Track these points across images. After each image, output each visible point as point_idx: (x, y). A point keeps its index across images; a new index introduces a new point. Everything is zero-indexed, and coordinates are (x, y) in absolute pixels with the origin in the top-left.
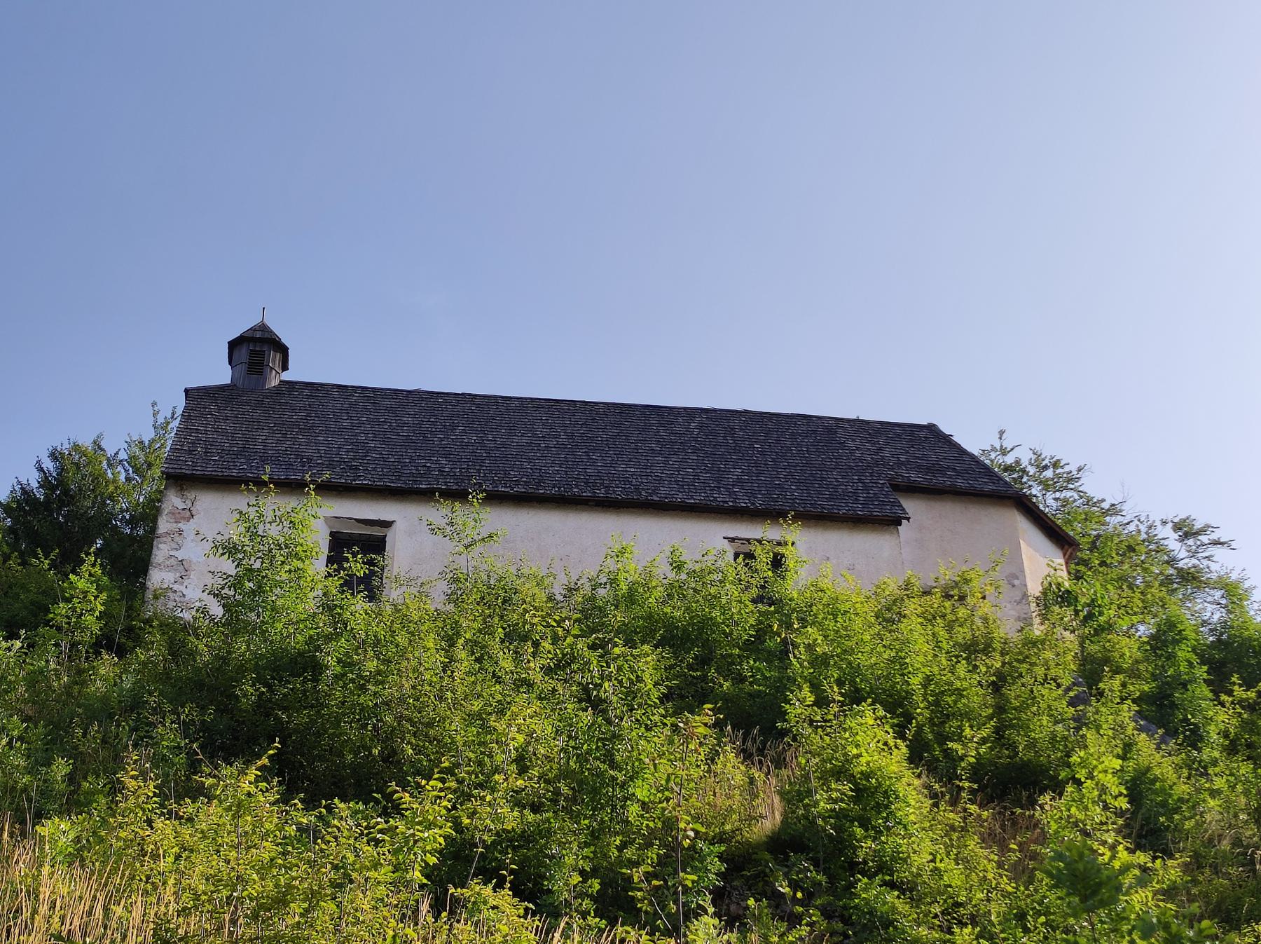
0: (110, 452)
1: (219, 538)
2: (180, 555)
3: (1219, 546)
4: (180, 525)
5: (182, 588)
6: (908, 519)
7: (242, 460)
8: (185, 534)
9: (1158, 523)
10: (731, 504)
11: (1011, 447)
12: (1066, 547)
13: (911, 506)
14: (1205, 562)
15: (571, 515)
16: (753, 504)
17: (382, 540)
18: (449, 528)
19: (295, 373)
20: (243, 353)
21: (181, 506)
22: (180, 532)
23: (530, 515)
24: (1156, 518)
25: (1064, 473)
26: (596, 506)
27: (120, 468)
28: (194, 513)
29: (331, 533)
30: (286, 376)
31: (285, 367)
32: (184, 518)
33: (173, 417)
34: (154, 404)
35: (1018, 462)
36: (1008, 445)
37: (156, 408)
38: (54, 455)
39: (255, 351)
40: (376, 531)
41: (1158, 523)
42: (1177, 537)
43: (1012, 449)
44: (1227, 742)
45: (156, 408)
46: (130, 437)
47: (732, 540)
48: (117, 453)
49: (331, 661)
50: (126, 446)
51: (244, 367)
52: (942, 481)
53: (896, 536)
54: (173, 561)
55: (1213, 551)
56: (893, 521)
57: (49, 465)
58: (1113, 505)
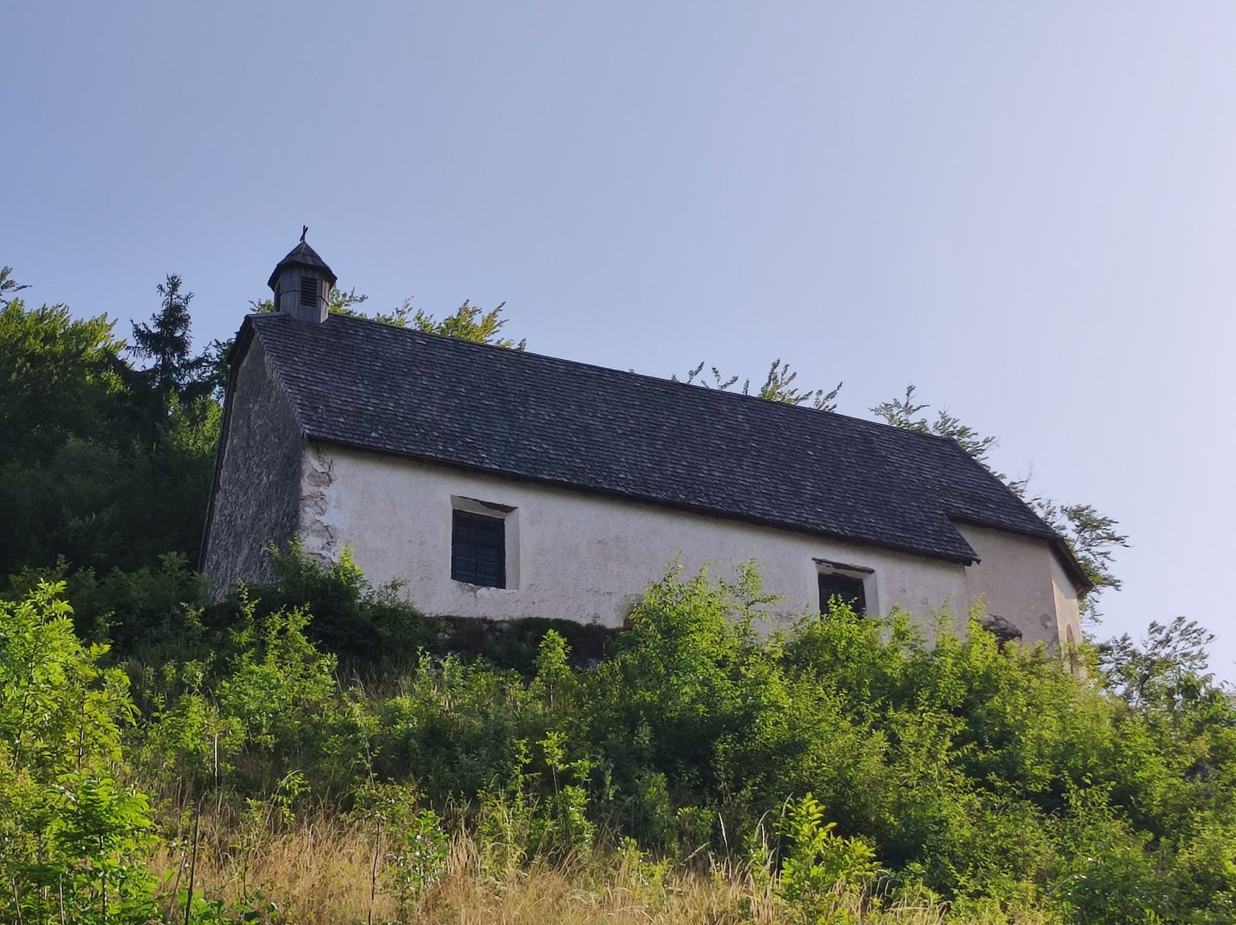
2: (325, 520)
3: (1113, 541)
4: (321, 489)
6: (978, 561)
9: (1058, 510)
11: (918, 406)
12: (1079, 586)
13: (975, 541)
14: (1101, 559)
15: (675, 519)
16: (842, 530)
17: (500, 525)
21: (320, 470)
23: (638, 516)
24: (1057, 505)
25: (970, 442)
26: (697, 513)
28: (332, 478)
29: (454, 510)
32: (323, 482)
35: (923, 423)
36: (914, 403)
39: (307, 278)
40: (496, 514)
41: (1058, 510)
42: (1075, 528)
43: (918, 408)
47: (819, 562)
51: (298, 295)
52: (986, 514)
53: (962, 571)
55: (1107, 546)
56: (962, 559)
58: (1014, 483)
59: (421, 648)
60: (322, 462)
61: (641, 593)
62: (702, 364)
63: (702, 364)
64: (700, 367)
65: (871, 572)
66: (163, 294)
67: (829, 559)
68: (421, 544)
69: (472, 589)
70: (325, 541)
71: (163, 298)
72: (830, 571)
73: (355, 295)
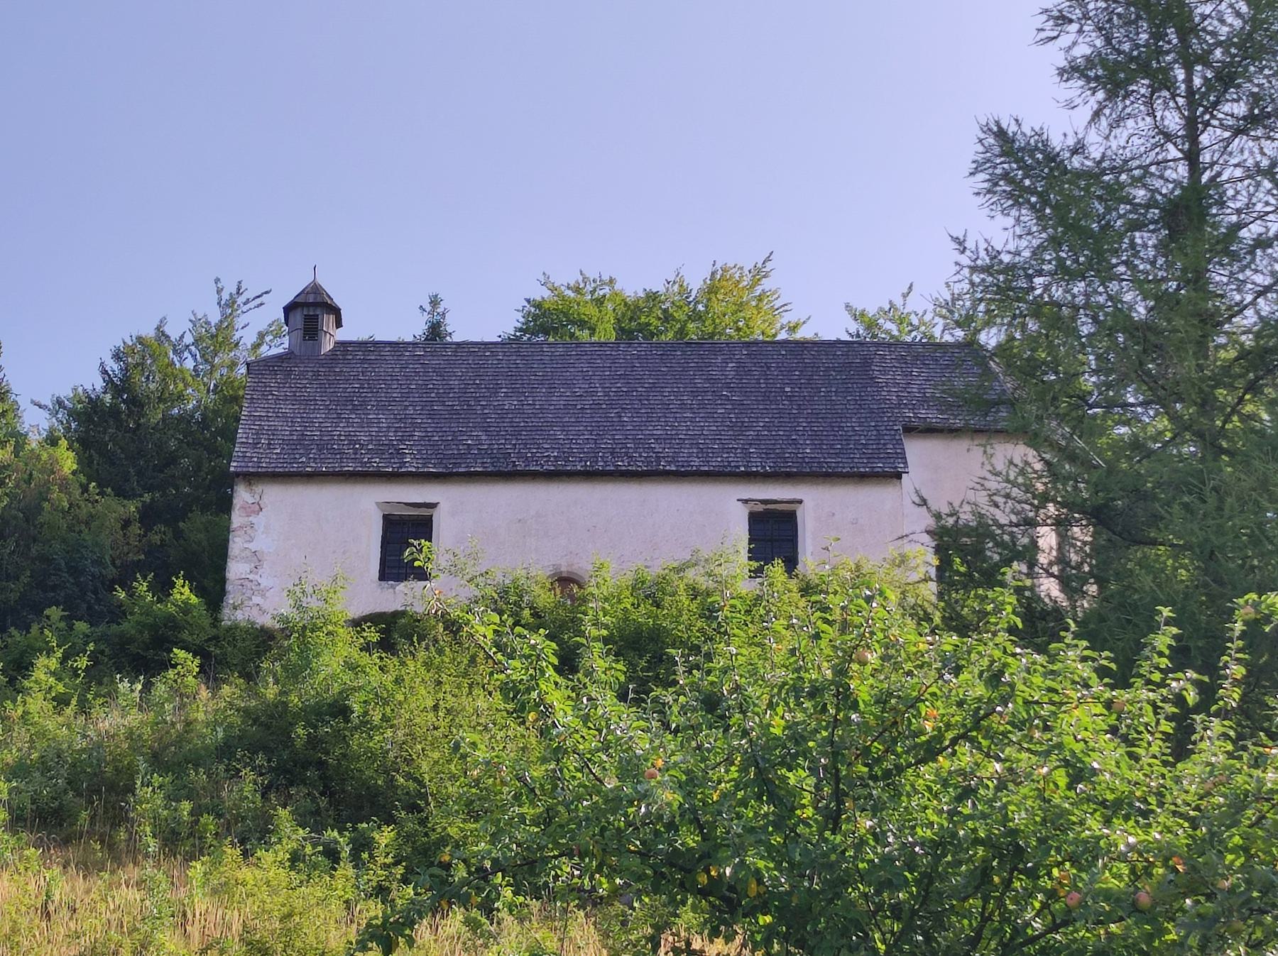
0: (174, 336)
1: (275, 612)
2: (253, 547)
4: (251, 519)
5: (257, 577)
7: (301, 451)
8: (256, 527)
10: (743, 469)
18: (453, 568)
19: (350, 331)
20: (298, 318)
22: (252, 525)
27: (186, 354)
30: (342, 335)
31: (339, 324)
32: (254, 512)
33: (238, 293)
34: (217, 281)
37: (219, 285)
38: (117, 356)
40: (424, 512)
44: (956, 748)
45: (219, 285)
46: (194, 315)
47: (746, 501)
48: (182, 337)
49: (356, 707)
50: (191, 325)
51: (300, 333)
54: (248, 553)
57: (112, 366)
59: (118, 676)
60: (253, 493)
61: (558, 562)
62: (911, 285)
63: (911, 285)
64: (910, 288)
65: (800, 502)
66: (425, 314)
67: (754, 498)
68: (344, 553)
69: (393, 587)
70: (253, 565)
71: (426, 317)
72: (760, 508)
73: (603, 278)
